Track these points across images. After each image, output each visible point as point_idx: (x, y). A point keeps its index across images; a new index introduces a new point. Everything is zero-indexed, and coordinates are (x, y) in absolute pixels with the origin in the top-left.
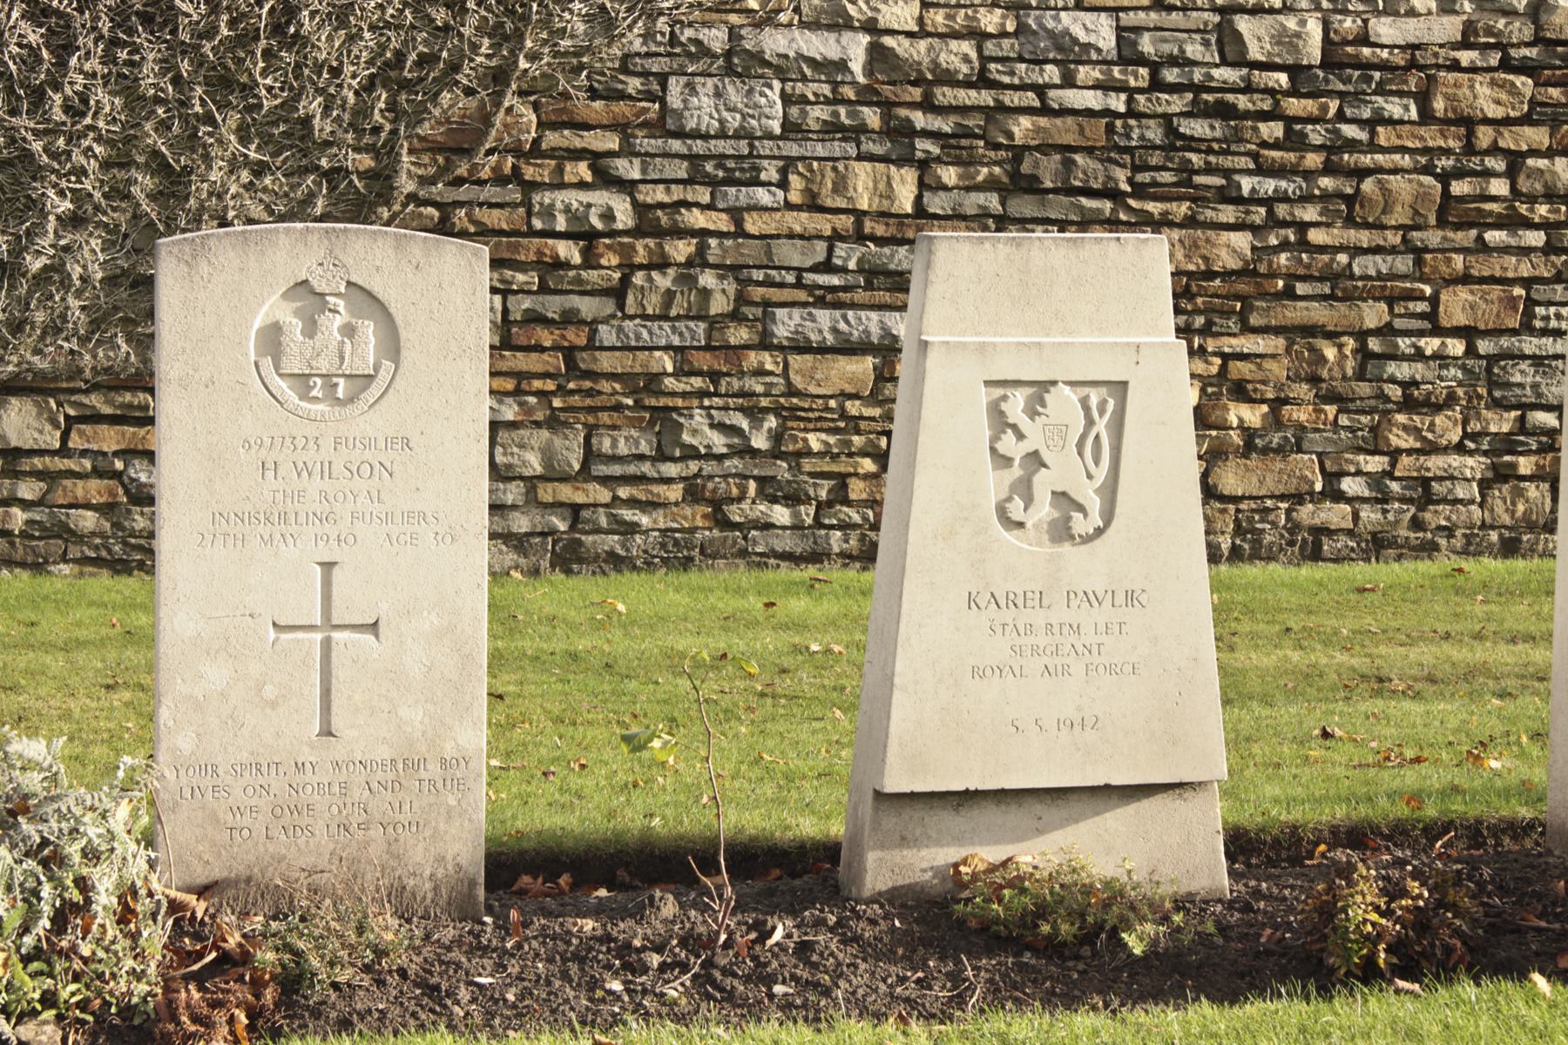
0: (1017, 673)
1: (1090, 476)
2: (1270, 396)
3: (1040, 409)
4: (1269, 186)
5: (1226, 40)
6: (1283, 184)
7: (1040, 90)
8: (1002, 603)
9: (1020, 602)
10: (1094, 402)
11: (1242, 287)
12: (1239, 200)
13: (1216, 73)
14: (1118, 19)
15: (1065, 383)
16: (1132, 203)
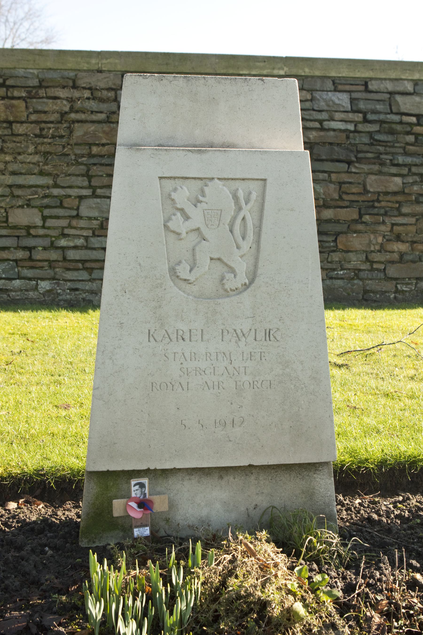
0: (185, 387)
1: (238, 247)
2: (410, 239)
3: (201, 198)
4: (409, 160)
5: (392, 104)
6: (415, 159)
7: (321, 122)
8: (174, 337)
9: (187, 337)
10: (241, 194)
11: (399, 198)
12: (398, 165)
13: (388, 116)
14: (350, 95)
15: (219, 179)
16: (357, 165)
